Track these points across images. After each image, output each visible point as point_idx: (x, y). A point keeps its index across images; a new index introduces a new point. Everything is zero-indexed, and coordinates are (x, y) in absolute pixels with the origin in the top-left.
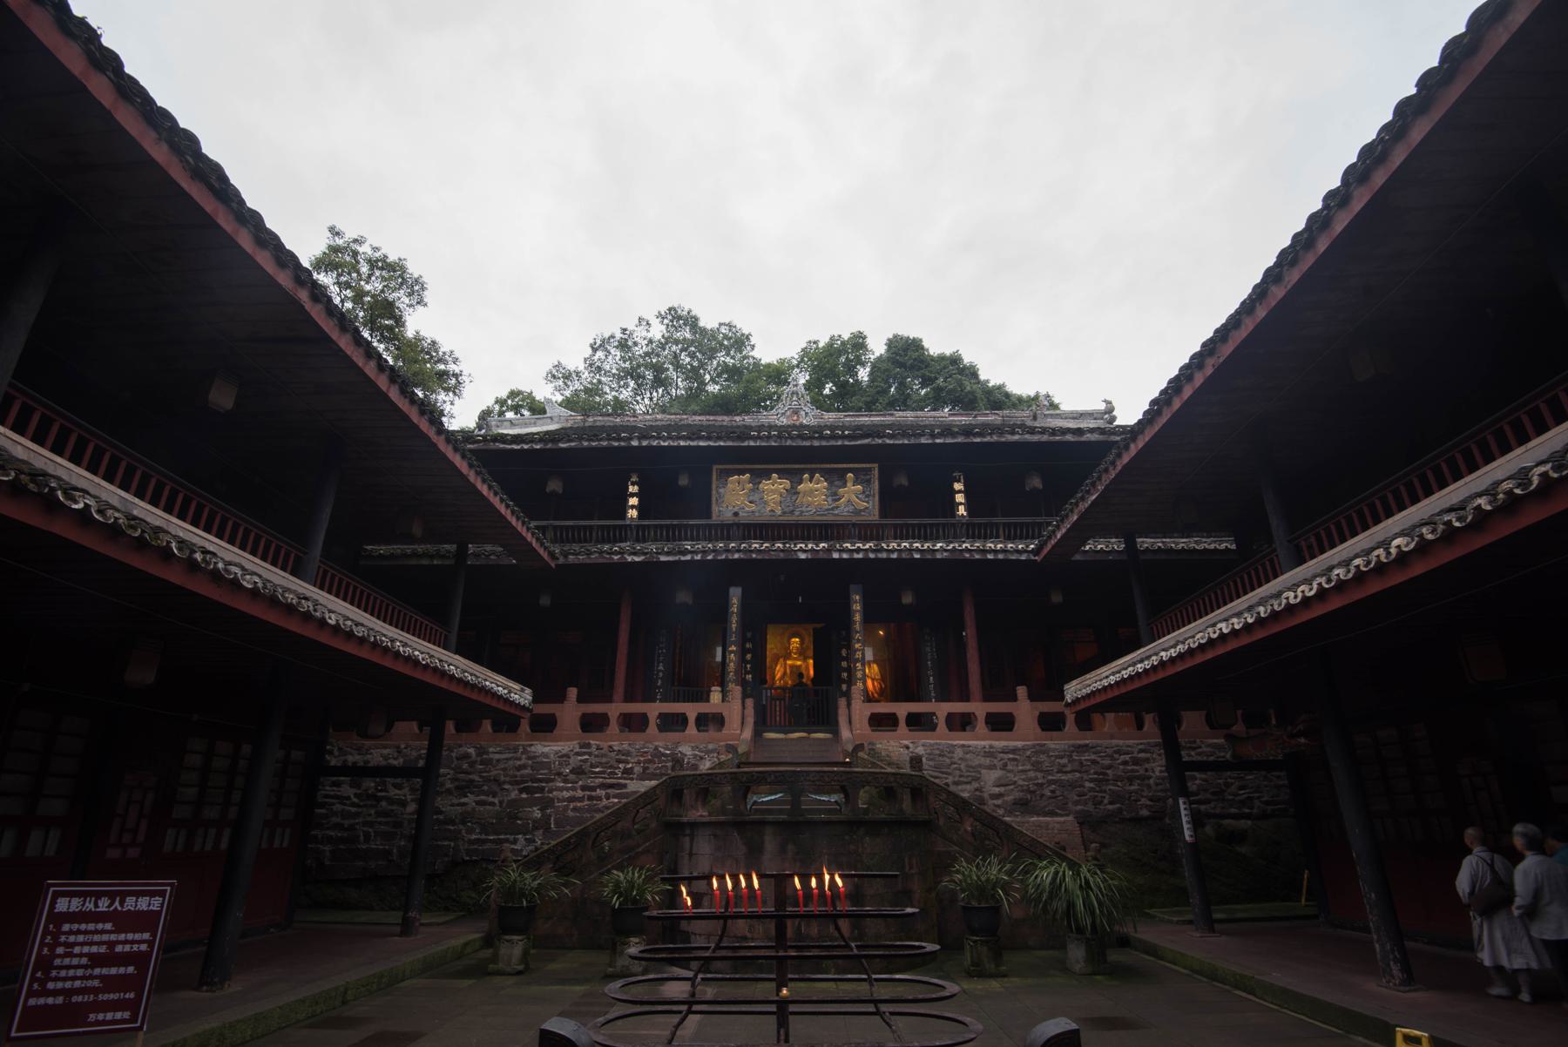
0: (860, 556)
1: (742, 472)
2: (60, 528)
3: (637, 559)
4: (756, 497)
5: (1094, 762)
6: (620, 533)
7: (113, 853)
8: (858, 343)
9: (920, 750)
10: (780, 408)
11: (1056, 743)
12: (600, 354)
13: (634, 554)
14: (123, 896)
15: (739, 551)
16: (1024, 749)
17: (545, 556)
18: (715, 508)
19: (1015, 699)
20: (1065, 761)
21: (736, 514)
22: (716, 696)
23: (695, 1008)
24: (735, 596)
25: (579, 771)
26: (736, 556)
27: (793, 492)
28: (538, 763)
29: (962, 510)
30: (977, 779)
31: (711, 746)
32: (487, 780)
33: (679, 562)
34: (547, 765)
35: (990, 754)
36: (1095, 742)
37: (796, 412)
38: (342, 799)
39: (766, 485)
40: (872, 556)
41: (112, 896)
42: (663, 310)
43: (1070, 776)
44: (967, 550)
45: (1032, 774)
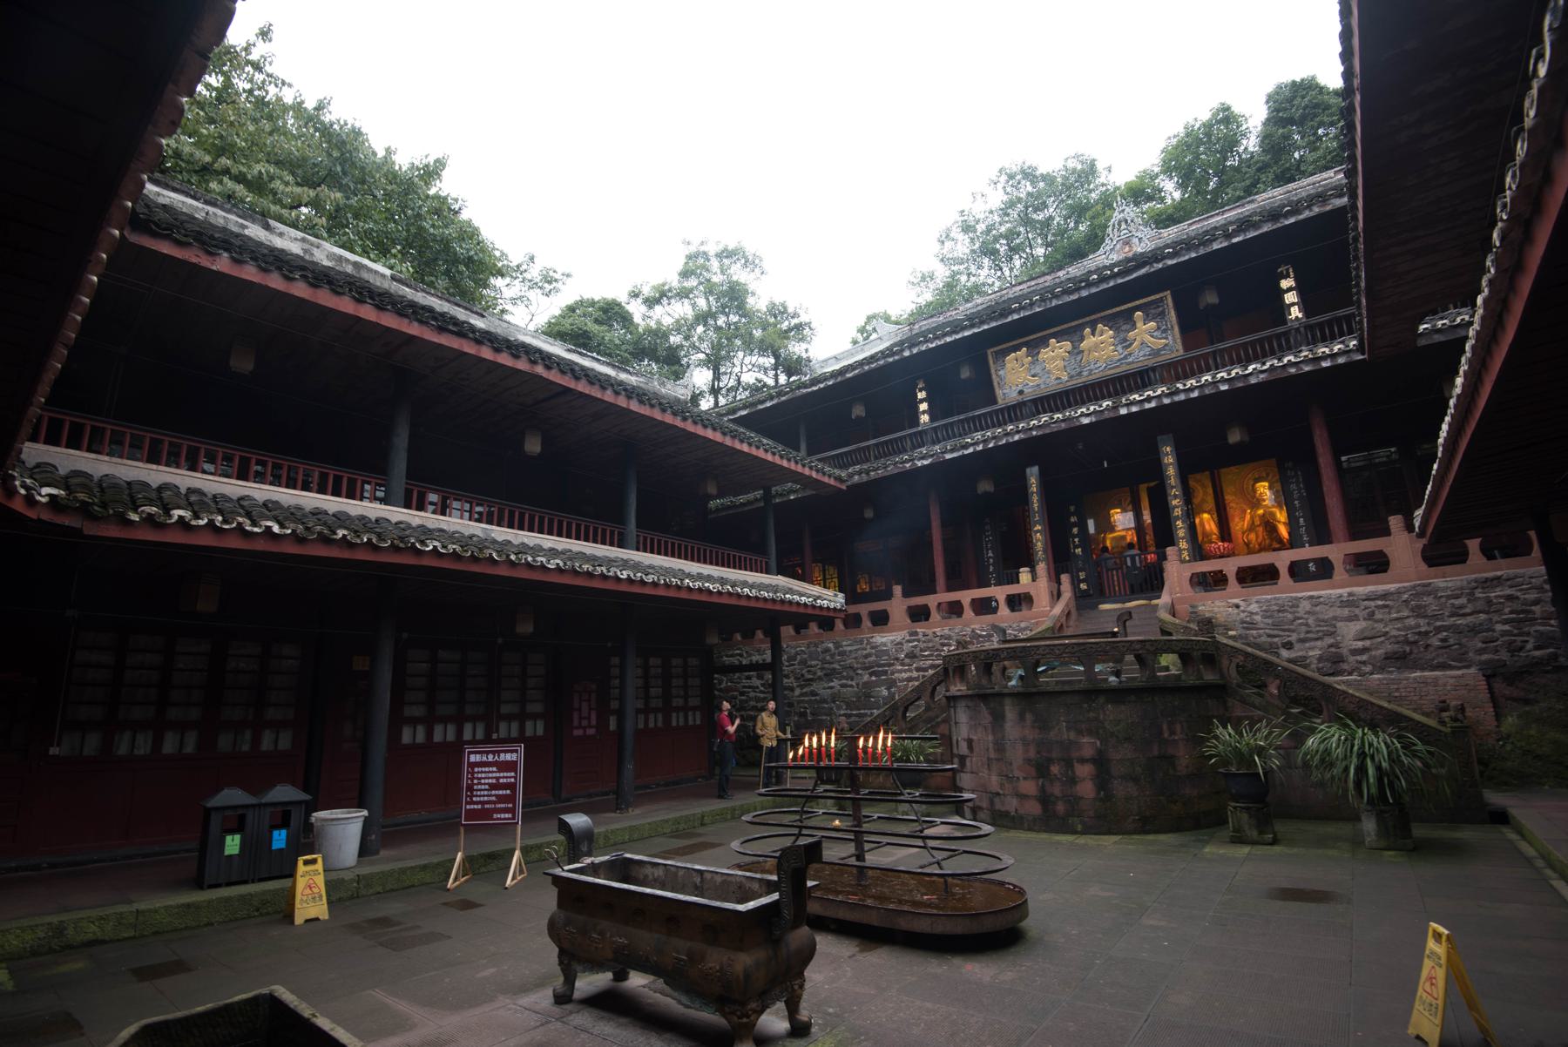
0: (1153, 404)
1: (1017, 348)
2: (426, 562)
3: (926, 462)
4: (1038, 369)
5: (1510, 598)
6: (920, 439)
7: (578, 732)
8: (1226, 117)
9: (1254, 607)
10: (1108, 245)
11: (1448, 580)
12: (948, 244)
13: (923, 458)
14: (499, 752)
15: (1018, 432)
16: (1399, 592)
17: (832, 482)
18: (999, 393)
19: (1386, 532)
20: (1463, 601)
21: (1021, 392)
22: (1025, 576)
23: (805, 832)
24: (1033, 476)
25: (912, 656)
26: (1017, 438)
27: (1076, 352)
28: (880, 652)
29: (1295, 312)
30: (1332, 634)
31: (1023, 625)
32: (845, 668)
33: (964, 456)
34: (886, 652)
35: (1350, 603)
36: (1511, 572)
37: (1127, 243)
38: (754, 688)
39: (1045, 353)
40: (1166, 401)
41: (493, 753)
42: (994, 175)
43: (1470, 619)
44: (1290, 364)
45: (1412, 622)
